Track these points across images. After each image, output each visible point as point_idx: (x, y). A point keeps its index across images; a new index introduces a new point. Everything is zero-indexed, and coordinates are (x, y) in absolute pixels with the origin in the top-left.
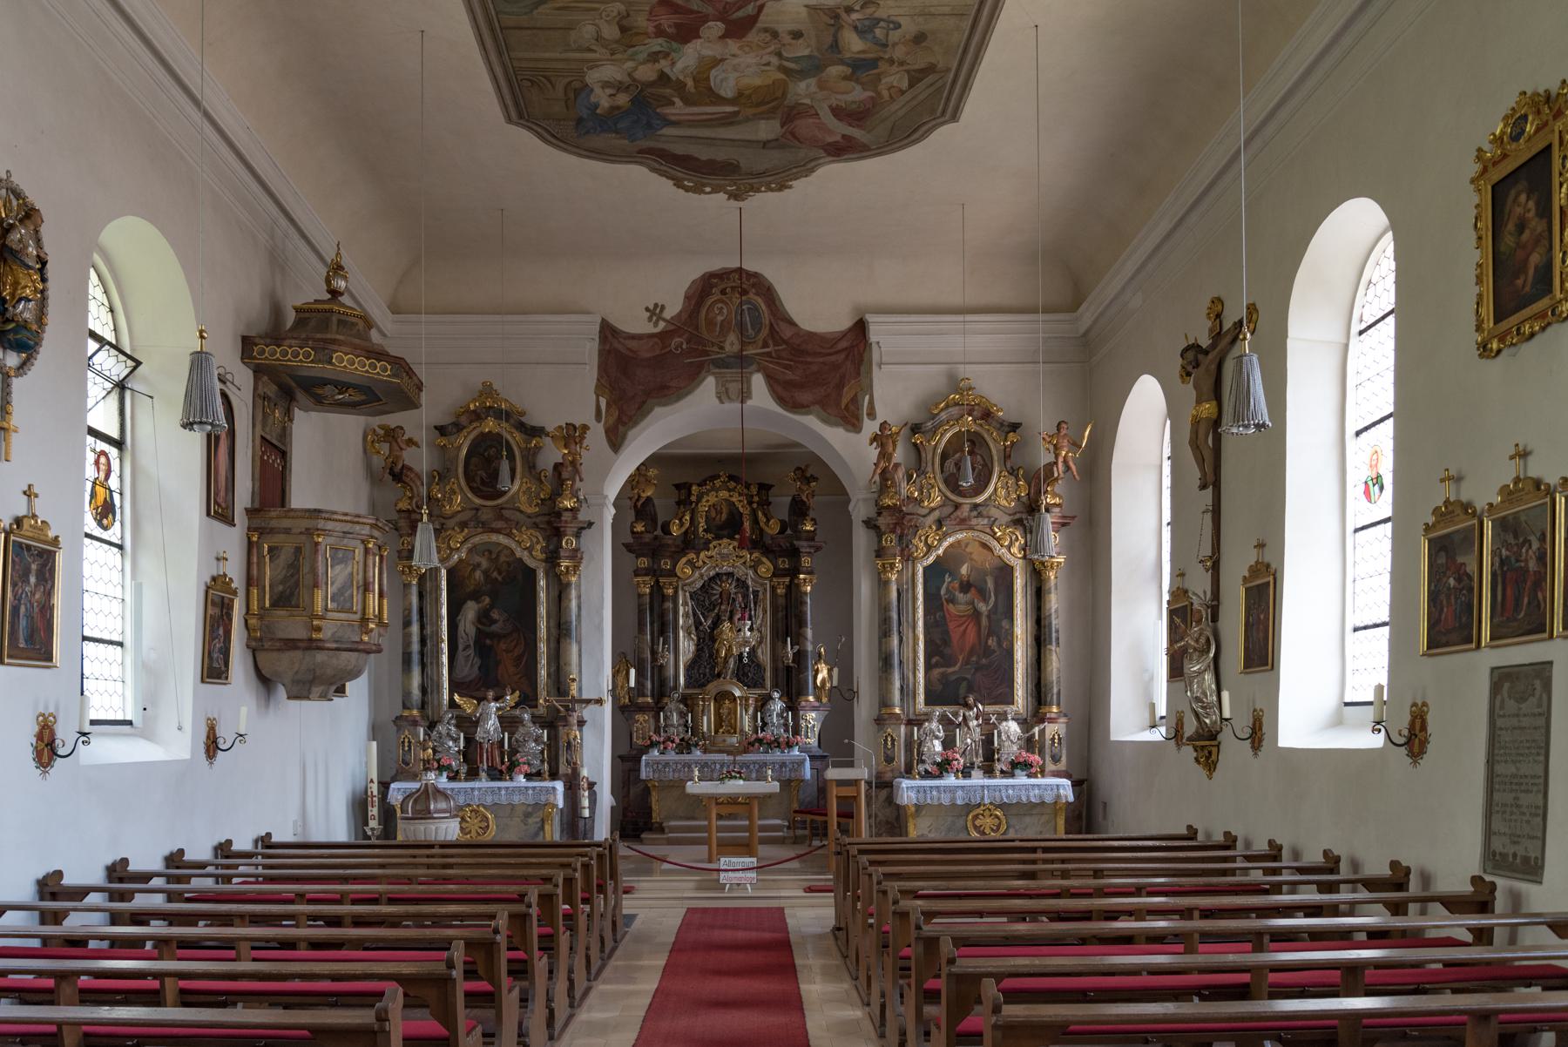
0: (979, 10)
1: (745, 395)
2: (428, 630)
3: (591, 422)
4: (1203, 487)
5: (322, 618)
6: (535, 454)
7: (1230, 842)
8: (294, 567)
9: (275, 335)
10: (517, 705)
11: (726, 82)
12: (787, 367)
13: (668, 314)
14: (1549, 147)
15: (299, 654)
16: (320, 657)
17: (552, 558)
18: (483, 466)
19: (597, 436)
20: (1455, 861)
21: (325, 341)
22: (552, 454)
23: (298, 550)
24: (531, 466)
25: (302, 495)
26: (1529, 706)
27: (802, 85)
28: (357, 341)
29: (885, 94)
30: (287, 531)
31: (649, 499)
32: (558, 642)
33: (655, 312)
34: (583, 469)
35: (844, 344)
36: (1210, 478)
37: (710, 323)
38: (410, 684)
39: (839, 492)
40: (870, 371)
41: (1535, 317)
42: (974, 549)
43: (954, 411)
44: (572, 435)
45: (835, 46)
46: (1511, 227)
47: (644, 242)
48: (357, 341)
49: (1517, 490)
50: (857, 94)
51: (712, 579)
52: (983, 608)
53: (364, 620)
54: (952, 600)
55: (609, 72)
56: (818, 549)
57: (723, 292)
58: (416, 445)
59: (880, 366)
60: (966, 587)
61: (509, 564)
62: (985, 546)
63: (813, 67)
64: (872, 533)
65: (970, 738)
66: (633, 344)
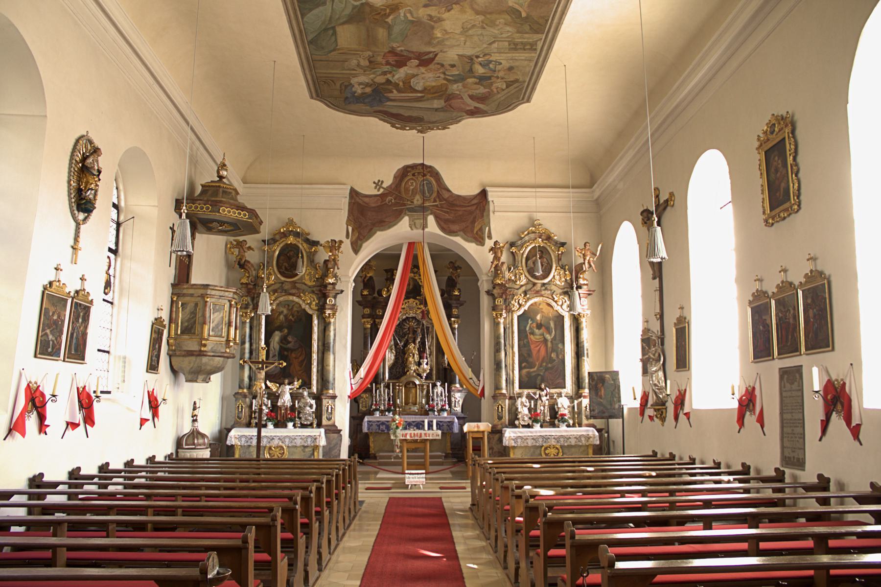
0: (538, 58)
1: (424, 226)
2: (254, 346)
3: (344, 239)
4: (654, 278)
5: (207, 340)
6: (314, 255)
7: (672, 457)
8: (194, 313)
9: (191, 199)
10: (300, 388)
11: (418, 84)
12: (445, 212)
13: (385, 185)
14: (784, 138)
15: (193, 358)
16: (205, 360)
17: (321, 309)
18: (288, 261)
19: (347, 245)
20: (768, 460)
21: (217, 202)
22: (323, 255)
23: (196, 305)
24: (311, 261)
25: (196, 278)
26: (795, 386)
27: (455, 86)
28: (232, 201)
29: (495, 90)
30: (192, 295)
31: (371, 277)
32: (323, 353)
33: (378, 184)
34: (339, 263)
35: (475, 201)
36: (657, 274)
37: (407, 190)
38: (243, 375)
39: (474, 277)
40: (489, 215)
41: (786, 210)
42: (544, 307)
43: (532, 236)
44: (334, 246)
45: (471, 70)
46: (773, 170)
47: (376, 151)
48: (232, 201)
49: (783, 287)
50: (481, 90)
51: (404, 320)
52: (548, 337)
53: (228, 341)
54: (533, 333)
55: (363, 79)
56: (462, 305)
57: (414, 175)
58: (252, 249)
59: (494, 212)
60: (539, 326)
61: (298, 312)
62: (549, 305)
63: (460, 79)
64: (491, 298)
65: (543, 408)
66: (366, 200)
